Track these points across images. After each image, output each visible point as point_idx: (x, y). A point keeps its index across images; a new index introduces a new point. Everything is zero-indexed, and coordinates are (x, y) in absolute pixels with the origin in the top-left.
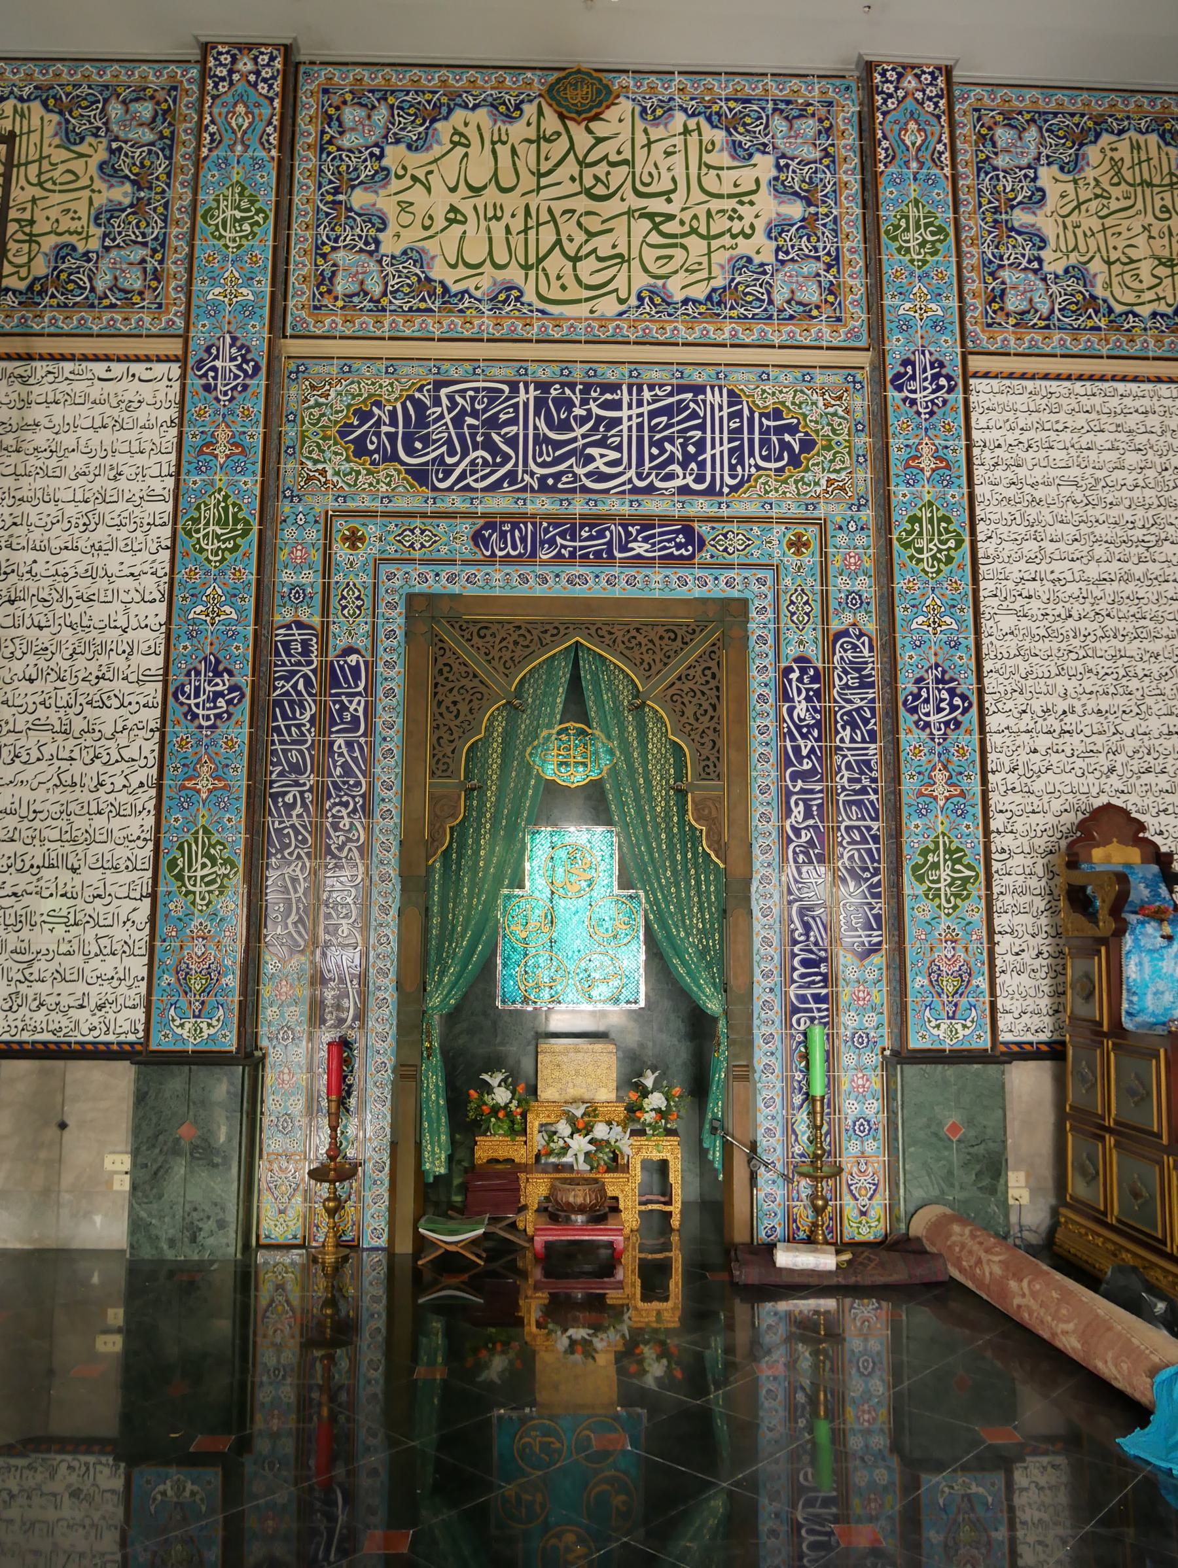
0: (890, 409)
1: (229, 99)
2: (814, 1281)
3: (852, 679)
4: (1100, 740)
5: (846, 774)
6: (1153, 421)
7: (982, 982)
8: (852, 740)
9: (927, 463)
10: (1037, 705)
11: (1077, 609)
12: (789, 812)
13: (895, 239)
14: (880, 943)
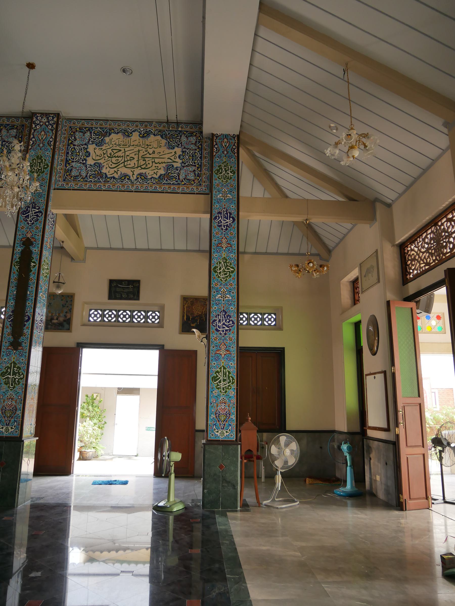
1: (40, 130)
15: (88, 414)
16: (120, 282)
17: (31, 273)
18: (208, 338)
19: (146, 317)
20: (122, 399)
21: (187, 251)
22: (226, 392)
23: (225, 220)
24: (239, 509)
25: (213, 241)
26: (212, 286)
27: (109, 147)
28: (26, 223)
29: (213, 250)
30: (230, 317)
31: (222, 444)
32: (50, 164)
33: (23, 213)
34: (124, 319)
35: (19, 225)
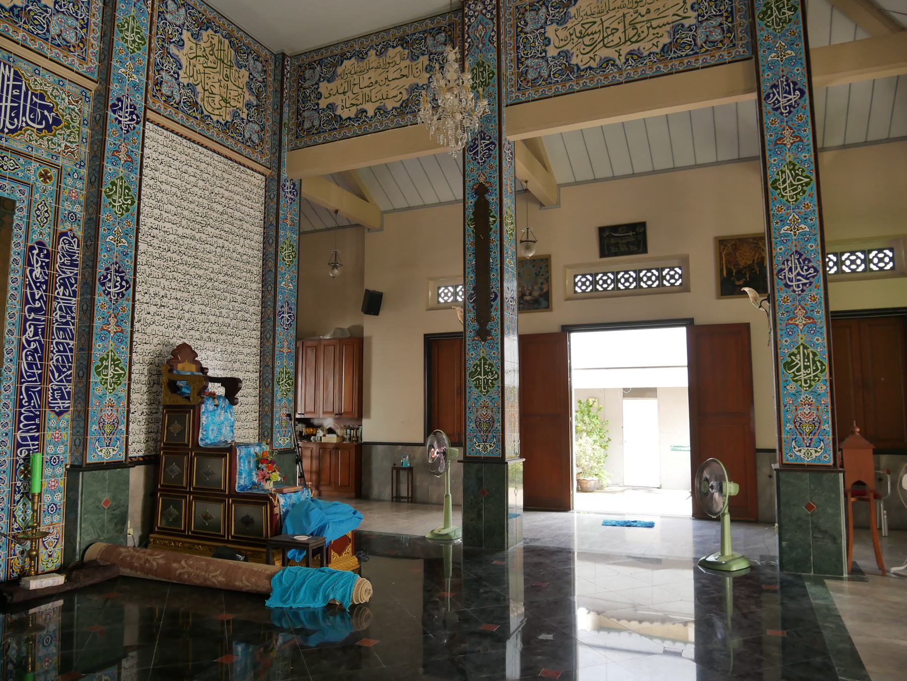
0: (108, 121)
2: (55, 592)
3: (67, 260)
4: (176, 312)
5: (59, 313)
6: (210, 169)
7: (123, 427)
8: (64, 294)
9: (122, 156)
10: (152, 290)
11: (173, 248)
12: (25, 331)
13: (121, 32)
14: (68, 407)
15: (585, 428)
16: (615, 228)
17: (491, 232)
18: (771, 299)
19: (661, 278)
20: (631, 405)
21: (717, 163)
22: (810, 386)
23: (786, 97)
24: (845, 575)
25: (767, 138)
26: (771, 213)
27: (576, 22)
28: (475, 162)
29: (768, 153)
30: (810, 261)
31: (807, 471)
32: (496, 71)
33: (471, 148)
34: (627, 284)
35: (467, 168)
